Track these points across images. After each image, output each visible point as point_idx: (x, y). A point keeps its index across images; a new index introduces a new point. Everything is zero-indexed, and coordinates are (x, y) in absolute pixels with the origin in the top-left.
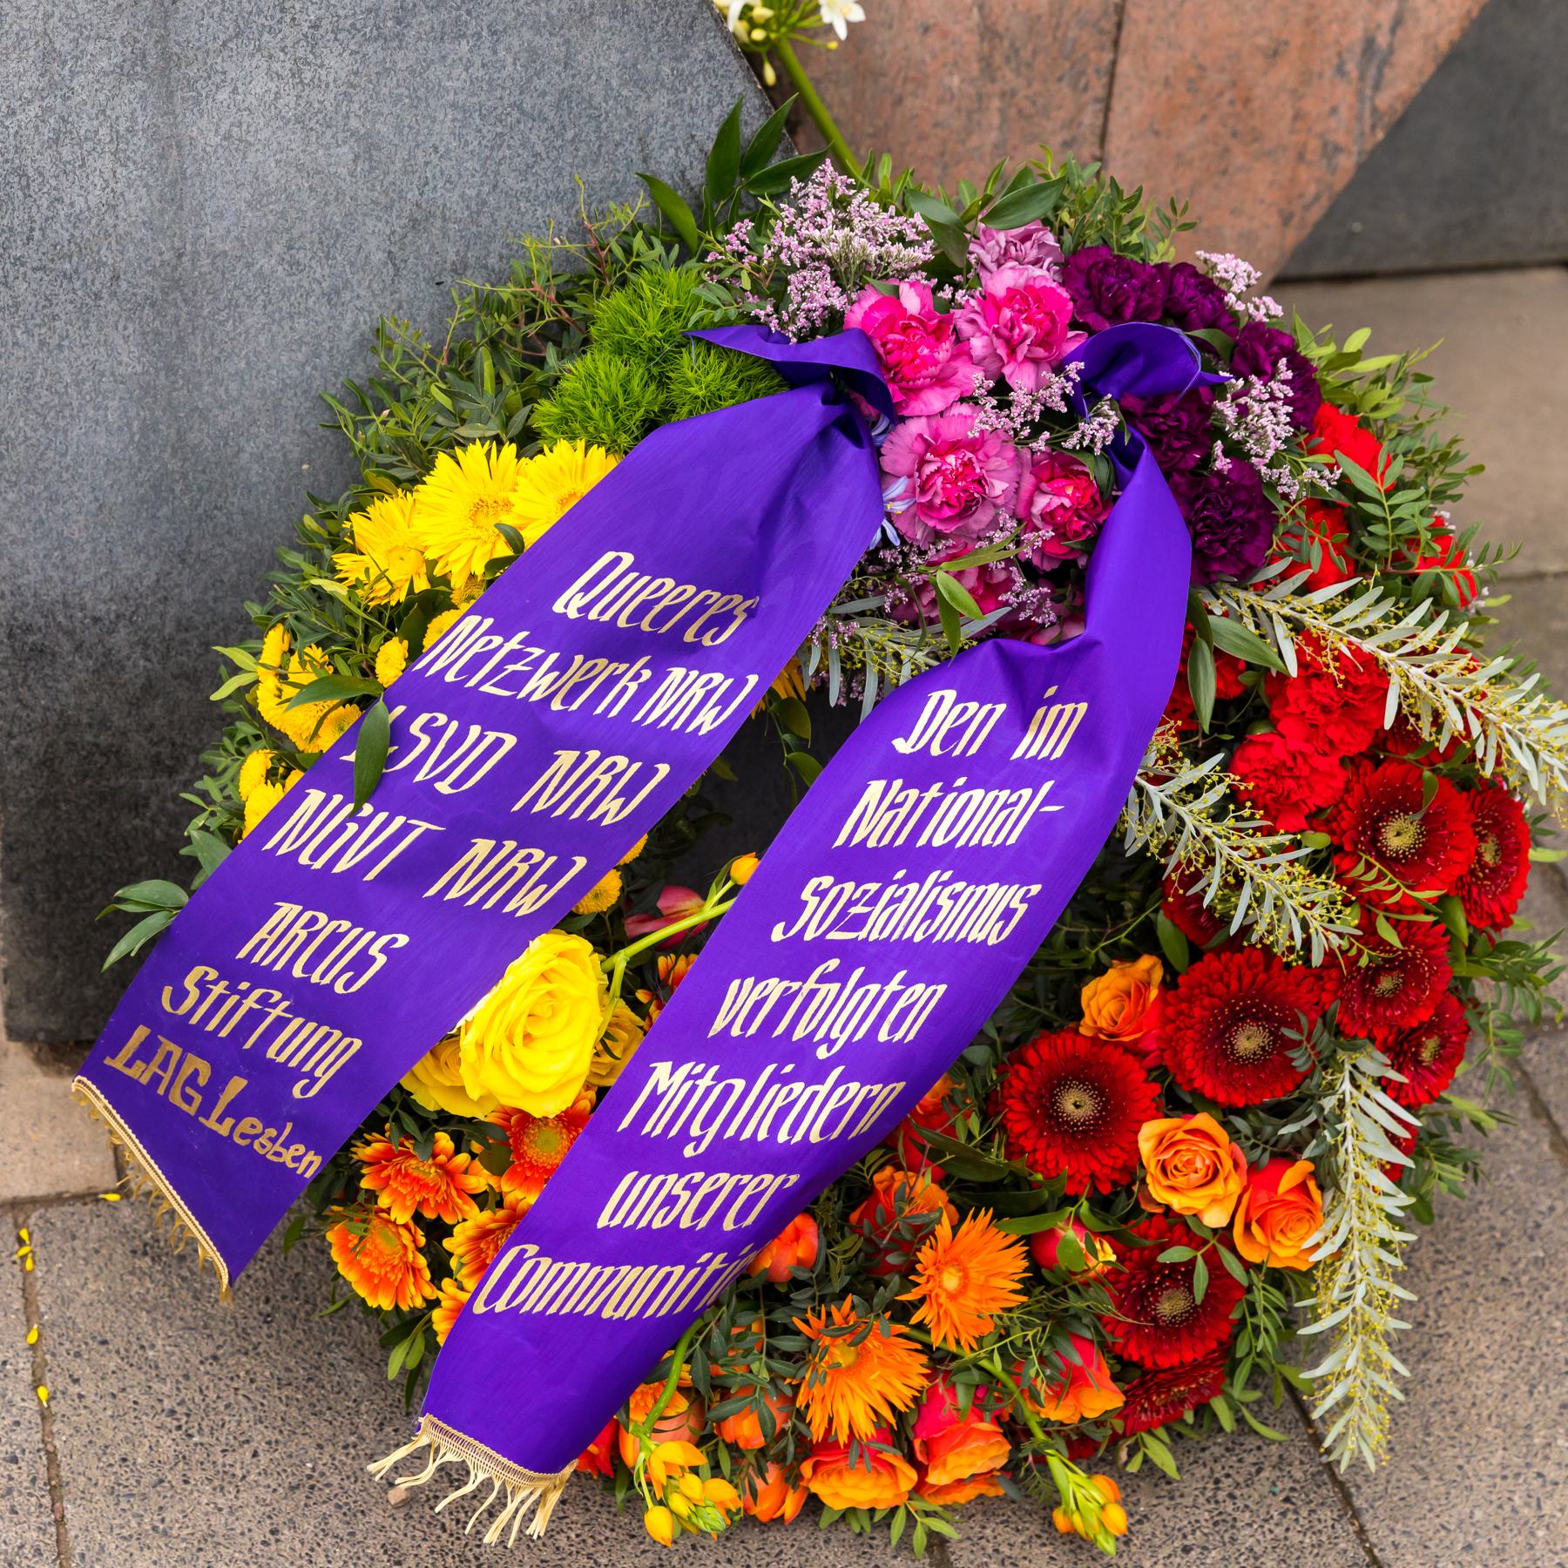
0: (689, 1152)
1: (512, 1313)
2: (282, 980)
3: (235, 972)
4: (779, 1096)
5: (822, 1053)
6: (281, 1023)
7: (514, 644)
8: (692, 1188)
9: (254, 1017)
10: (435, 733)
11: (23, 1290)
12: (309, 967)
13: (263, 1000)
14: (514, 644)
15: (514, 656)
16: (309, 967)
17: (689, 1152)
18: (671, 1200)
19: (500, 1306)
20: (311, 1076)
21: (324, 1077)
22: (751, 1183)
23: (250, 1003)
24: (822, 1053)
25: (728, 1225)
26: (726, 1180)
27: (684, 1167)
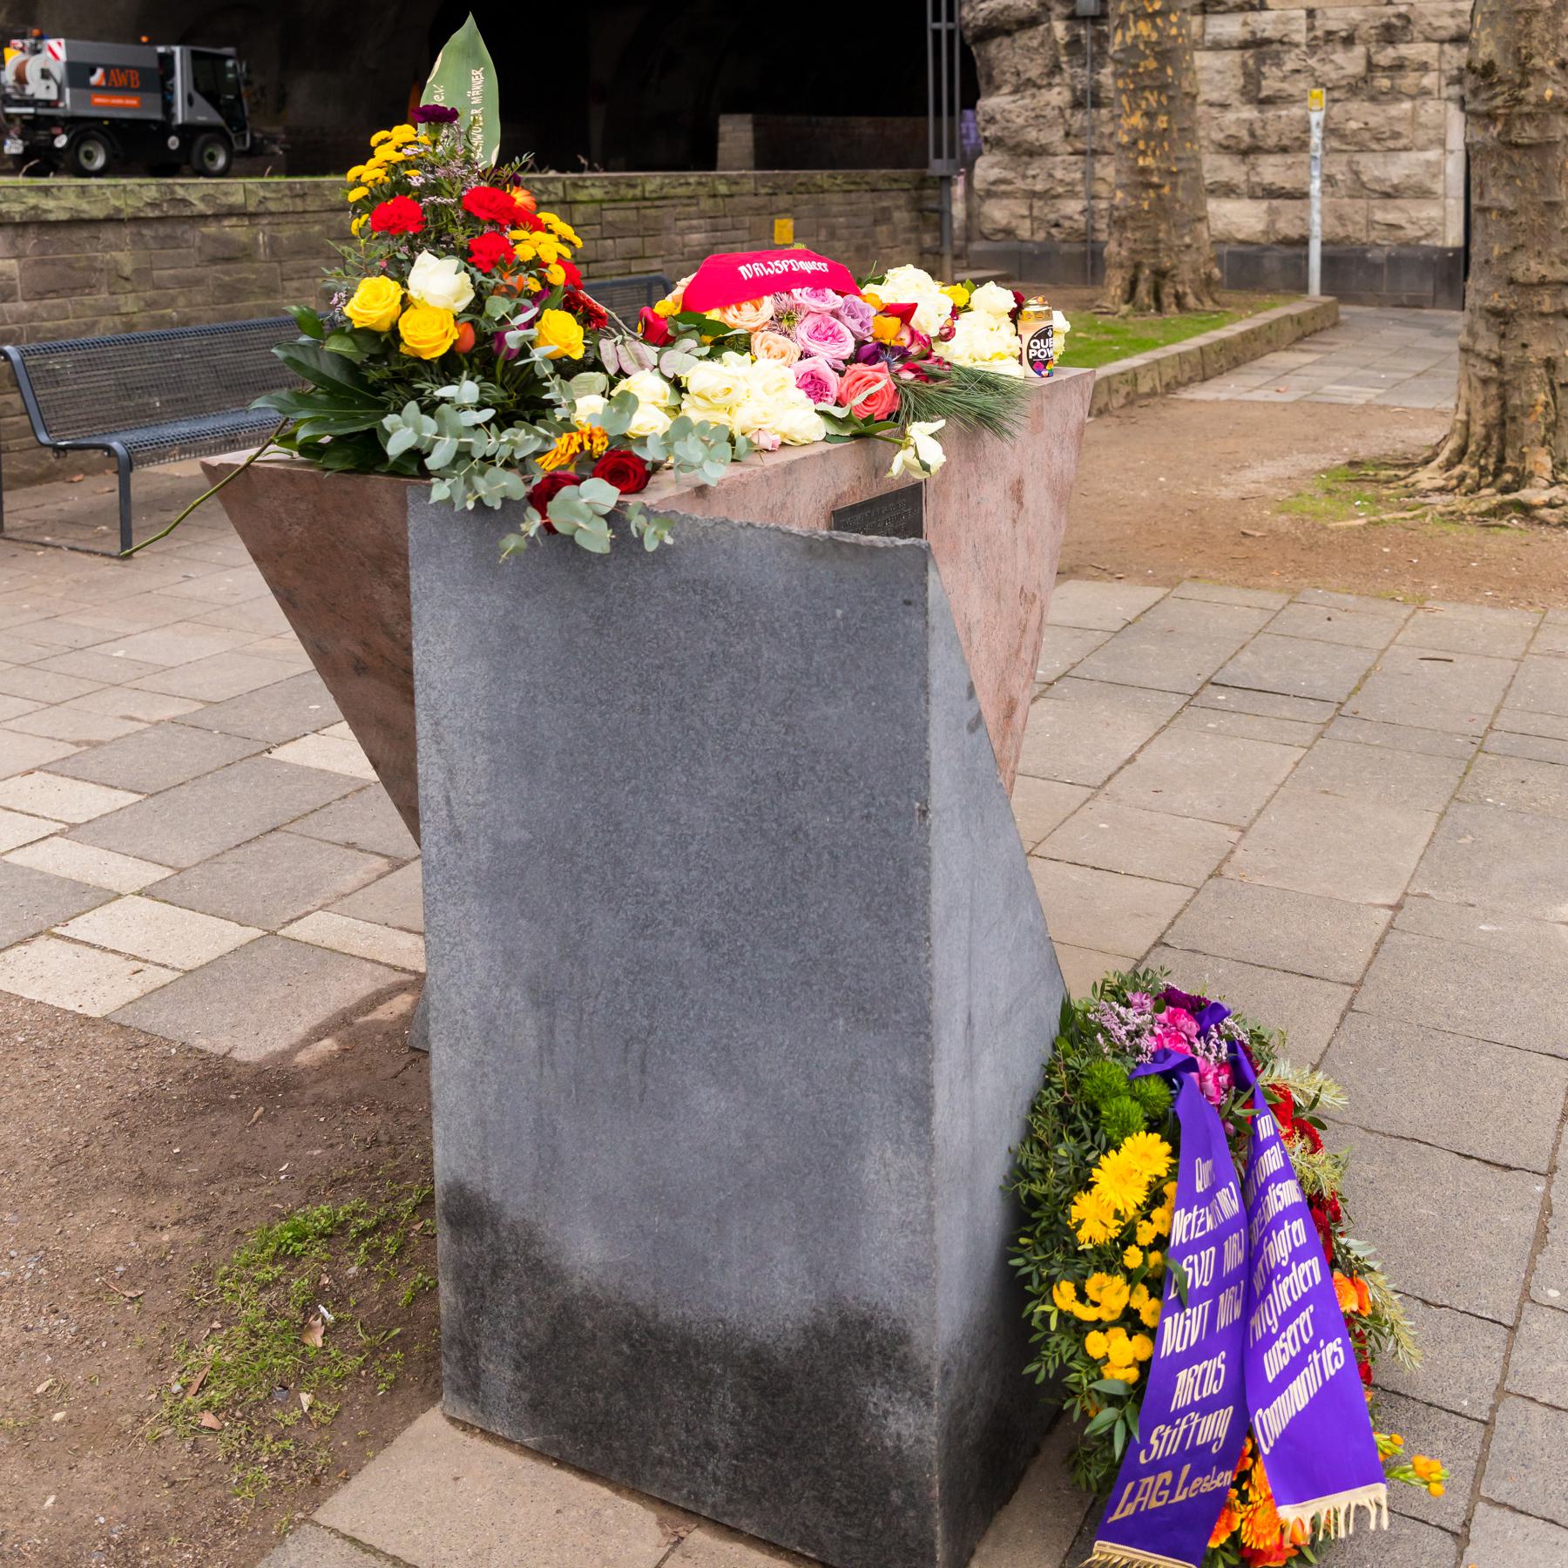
0: (1274, 1331)
1: (1276, 1441)
2: (1194, 1406)
3: (1170, 1420)
4: (1283, 1287)
5: (1284, 1263)
6: (1198, 1425)
7: (1195, 1213)
8: (1285, 1340)
9: (1187, 1432)
10: (1191, 1265)
11: (783, 445)
12: (1200, 1392)
13: (1189, 1421)
14: (1195, 1213)
15: (1198, 1217)
16: (1200, 1392)
17: (1274, 1331)
18: (1283, 1351)
19: (1271, 1443)
20: (1218, 1439)
21: (1222, 1435)
22: (1300, 1321)
23: (1183, 1426)
24: (1284, 1263)
25: (1306, 1341)
26: (1292, 1328)
27: (1277, 1337)
